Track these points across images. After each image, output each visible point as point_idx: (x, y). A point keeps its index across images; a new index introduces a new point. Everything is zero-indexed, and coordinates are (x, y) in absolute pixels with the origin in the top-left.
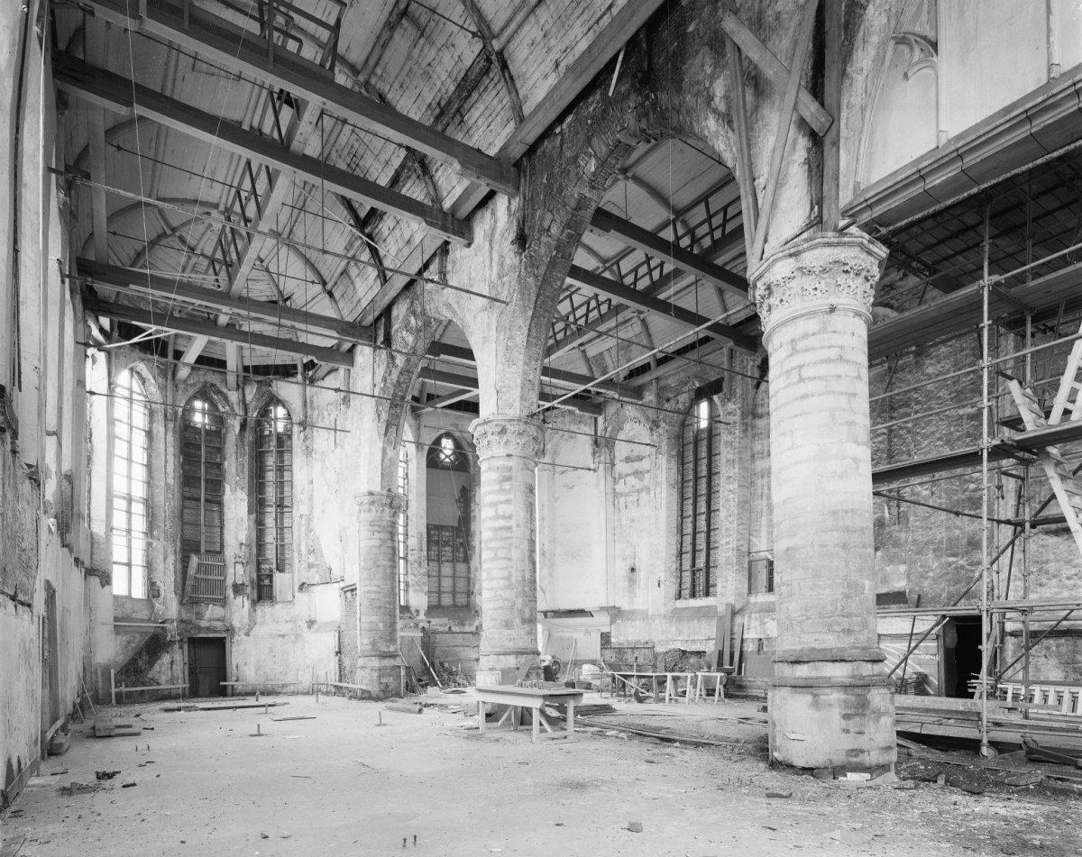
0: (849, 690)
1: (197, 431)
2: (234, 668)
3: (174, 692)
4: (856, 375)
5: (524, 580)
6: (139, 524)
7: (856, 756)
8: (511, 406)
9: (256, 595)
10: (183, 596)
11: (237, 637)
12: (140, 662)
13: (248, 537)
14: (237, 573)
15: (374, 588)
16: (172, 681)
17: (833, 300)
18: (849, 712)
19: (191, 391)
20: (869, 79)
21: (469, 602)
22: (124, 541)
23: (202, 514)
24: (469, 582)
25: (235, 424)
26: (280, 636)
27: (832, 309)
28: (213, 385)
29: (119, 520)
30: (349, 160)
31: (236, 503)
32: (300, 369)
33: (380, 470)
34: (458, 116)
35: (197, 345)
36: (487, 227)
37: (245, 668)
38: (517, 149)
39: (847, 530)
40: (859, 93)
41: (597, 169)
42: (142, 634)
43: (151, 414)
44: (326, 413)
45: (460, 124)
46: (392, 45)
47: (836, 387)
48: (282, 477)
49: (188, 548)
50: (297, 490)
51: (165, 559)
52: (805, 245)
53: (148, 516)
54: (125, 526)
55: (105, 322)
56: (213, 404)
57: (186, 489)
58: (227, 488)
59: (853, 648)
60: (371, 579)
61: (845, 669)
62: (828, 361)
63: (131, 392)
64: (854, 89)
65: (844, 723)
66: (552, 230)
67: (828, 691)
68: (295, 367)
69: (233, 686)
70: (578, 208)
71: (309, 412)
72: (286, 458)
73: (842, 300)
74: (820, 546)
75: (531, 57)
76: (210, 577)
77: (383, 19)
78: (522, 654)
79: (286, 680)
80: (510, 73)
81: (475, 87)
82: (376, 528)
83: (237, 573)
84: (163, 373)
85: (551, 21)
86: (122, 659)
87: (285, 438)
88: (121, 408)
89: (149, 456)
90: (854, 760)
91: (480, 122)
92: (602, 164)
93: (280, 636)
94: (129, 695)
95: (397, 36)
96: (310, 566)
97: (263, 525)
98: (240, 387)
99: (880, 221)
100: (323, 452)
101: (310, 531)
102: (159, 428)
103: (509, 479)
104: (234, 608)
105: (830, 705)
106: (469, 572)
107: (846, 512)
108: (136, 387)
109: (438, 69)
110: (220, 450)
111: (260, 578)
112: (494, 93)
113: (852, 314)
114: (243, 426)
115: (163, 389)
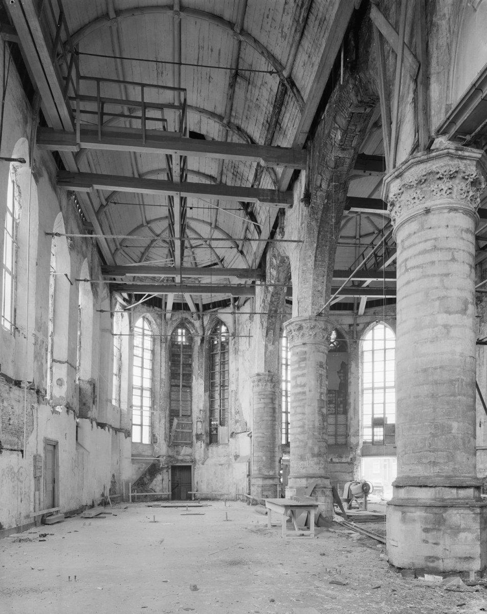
0: (428, 510)
1: (179, 346)
2: (196, 484)
3: (163, 496)
4: (450, 258)
5: (314, 428)
6: (147, 402)
7: (433, 561)
8: (306, 310)
9: (208, 441)
10: (169, 442)
11: (197, 466)
12: (145, 479)
13: (204, 406)
14: (199, 427)
15: (261, 435)
16: (162, 490)
17: (428, 204)
18: (428, 527)
19: (175, 324)
20: (451, 20)
21: (346, 441)
22: (139, 413)
23: (181, 394)
24: (347, 427)
25: (198, 340)
26: (220, 465)
27: (428, 211)
28: (186, 319)
29: (136, 401)
30: (232, 171)
31: (198, 385)
32: (232, 301)
33: (264, 359)
34: (278, 125)
35: (171, 299)
36: (298, 192)
37: (201, 484)
38: (300, 139)
39: (436, 383)
40: (445, 33)
41: (342, 136)
42: (147, 463)
43: (154, 341)
44: (245, 326)
45: (280, 130)
46: (236, 96)
47: (430, 270)
48: (224, 368)
49: (173, 414)
50: (231, 376)
51: (160, 421)
52: (403, 167)
53: (152, 398)
54: (139, 404)
55: (125, 295)
56: (188, 330)
57: (173, 380)
58: (194, 377)
59: (438, 476)
60: (258, 429)
61: (430, 493)
62: (425, 252)
63: (143, 329)
64: (440, 32)
65: (424, 535)
66: (323, 187)
67: (413, 509)
68: (230, 299)
69: (194, 494)
70: (336, 166)
71: (237, 327)
72: (226, 356)
73: (438, 201)
74: (414, 397)
75: (305, 73)
76: (185, 431)
77: (227, 83)
78: (311, 477)
79: (224, 491)
80: (297, 88)
81: (282, 104)
82: (263, 396)
83: (199, 427)
84: (160, 316)
85: (310, 46)
86: (136, 477)
87: (225, 344)
88: (137, 341)
89: (153, 364)
90: (431, 565)
91: (289, 125)
92: (345, 132)
93: (220, 465)
94: (139, 497)
95: (237, 89)
96: (237, 422)
97: (214, 398)
98: (200, 317)
99: (463, 131)
100: (243, 351)
101: (236, 400)
102: (158, 348)
103: (304, 359)
104: (196, 448)
105: (414, 520)
106: (347, 420)
107: (436, 369)
108: (146, 326)
109: (262, 100)
110: (190, 356)
111: (211, 431)
112: (292, 103)
113: (446, 211)
114: (202, 341)
115: (159, 325)
